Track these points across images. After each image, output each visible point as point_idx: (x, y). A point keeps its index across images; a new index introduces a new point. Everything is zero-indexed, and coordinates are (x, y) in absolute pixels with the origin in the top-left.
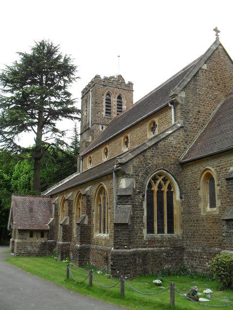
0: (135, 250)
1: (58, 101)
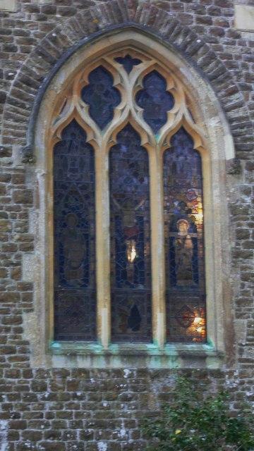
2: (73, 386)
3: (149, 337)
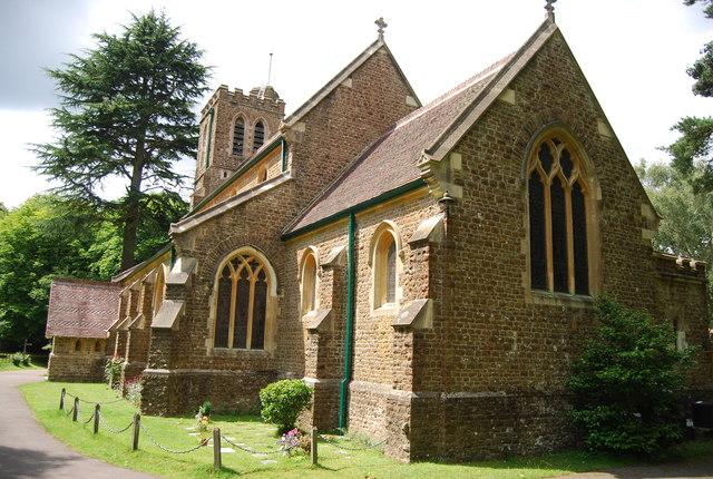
0: (185, 371)
1: (172, 124)
2: (543, 314)
3: (245, 347)
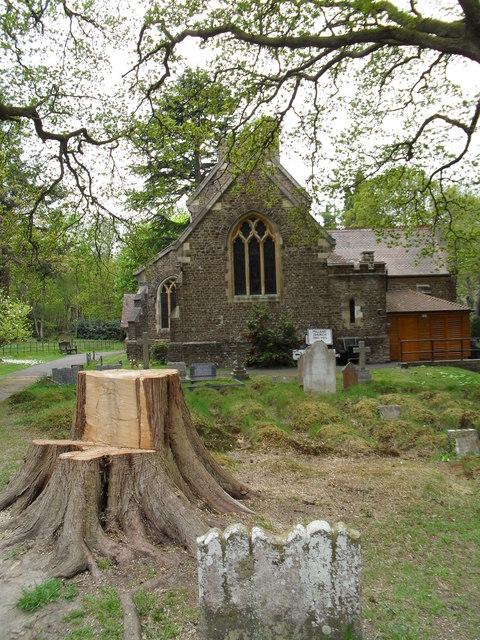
3: (245, 294)
